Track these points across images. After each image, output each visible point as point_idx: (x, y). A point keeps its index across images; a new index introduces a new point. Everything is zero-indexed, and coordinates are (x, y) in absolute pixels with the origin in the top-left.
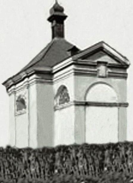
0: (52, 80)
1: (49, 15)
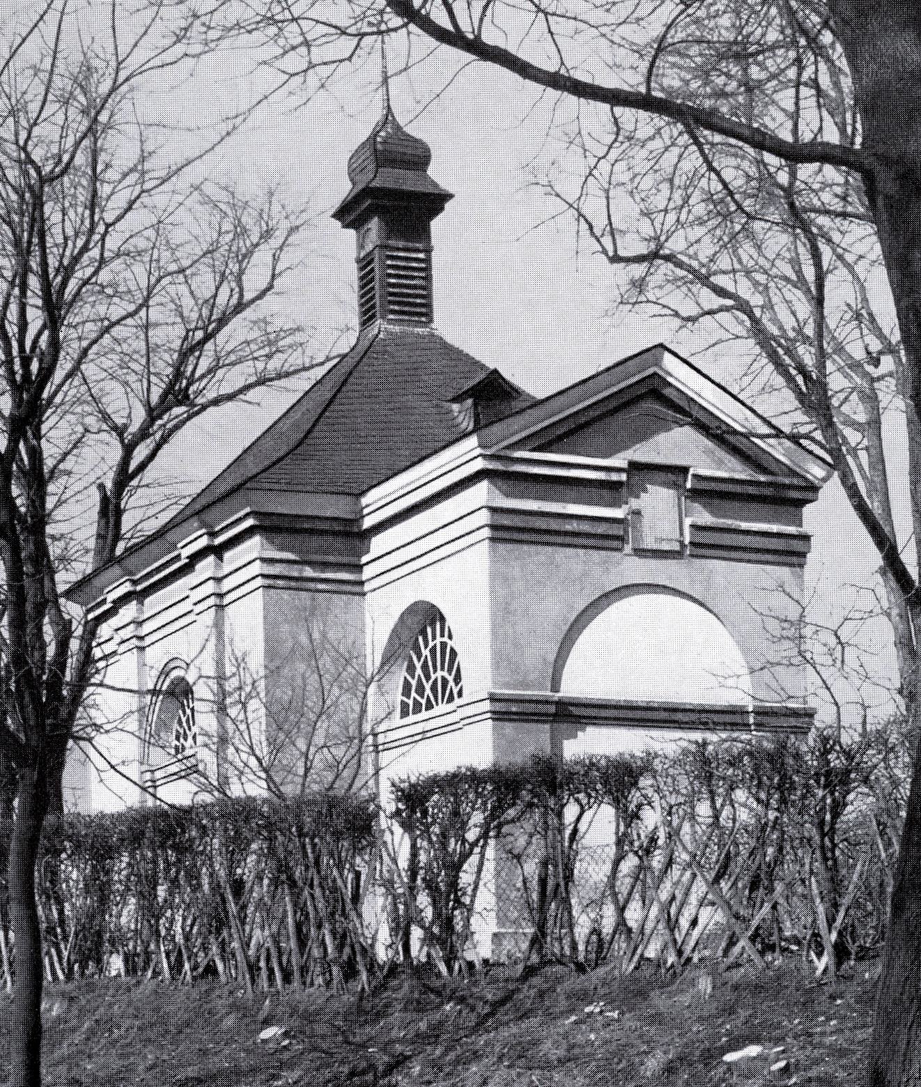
0: (359, 568)
1: (343, 189)
